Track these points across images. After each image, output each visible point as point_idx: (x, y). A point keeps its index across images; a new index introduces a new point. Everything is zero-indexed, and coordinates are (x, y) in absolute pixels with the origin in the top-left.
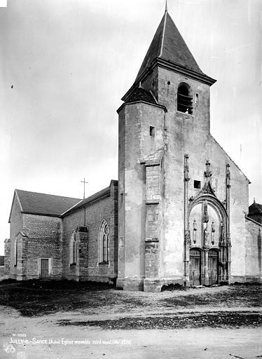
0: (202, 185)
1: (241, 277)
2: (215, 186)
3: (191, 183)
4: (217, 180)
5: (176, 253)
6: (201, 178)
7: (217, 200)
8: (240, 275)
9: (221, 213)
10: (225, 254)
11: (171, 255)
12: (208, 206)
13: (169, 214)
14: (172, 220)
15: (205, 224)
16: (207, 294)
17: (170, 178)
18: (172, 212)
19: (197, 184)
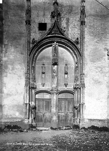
0: (49, 27)
1: (100, 120)
2: (65, 26)
3: (35, 27)
4: (68, 20)
5: (17, 96)
6: (48, 21)
7: (69, 41)
8: (100, 118)
9: (75, 54)
10: (79, 96)
11: (10, 98)
12: (60, 49)
13: (9, 59)
14: (12, 64)
15: (66, 76)
16: (45, 103)
17: (9, 24)
18: (12, 57)
19: (42, 27)
